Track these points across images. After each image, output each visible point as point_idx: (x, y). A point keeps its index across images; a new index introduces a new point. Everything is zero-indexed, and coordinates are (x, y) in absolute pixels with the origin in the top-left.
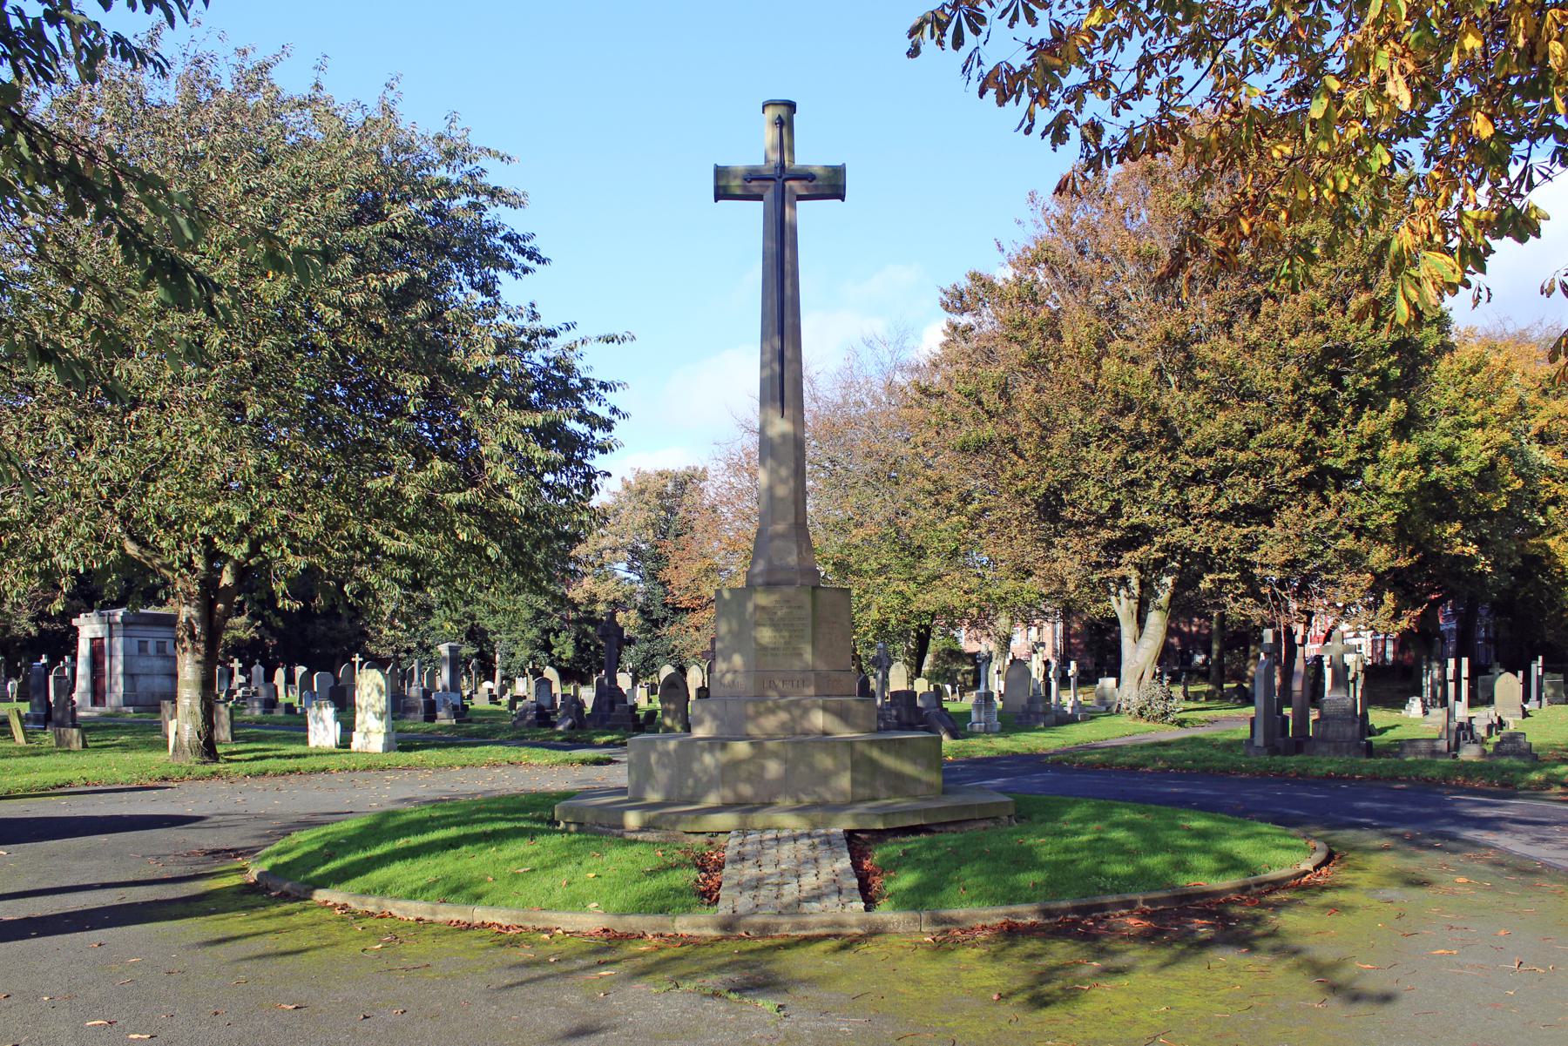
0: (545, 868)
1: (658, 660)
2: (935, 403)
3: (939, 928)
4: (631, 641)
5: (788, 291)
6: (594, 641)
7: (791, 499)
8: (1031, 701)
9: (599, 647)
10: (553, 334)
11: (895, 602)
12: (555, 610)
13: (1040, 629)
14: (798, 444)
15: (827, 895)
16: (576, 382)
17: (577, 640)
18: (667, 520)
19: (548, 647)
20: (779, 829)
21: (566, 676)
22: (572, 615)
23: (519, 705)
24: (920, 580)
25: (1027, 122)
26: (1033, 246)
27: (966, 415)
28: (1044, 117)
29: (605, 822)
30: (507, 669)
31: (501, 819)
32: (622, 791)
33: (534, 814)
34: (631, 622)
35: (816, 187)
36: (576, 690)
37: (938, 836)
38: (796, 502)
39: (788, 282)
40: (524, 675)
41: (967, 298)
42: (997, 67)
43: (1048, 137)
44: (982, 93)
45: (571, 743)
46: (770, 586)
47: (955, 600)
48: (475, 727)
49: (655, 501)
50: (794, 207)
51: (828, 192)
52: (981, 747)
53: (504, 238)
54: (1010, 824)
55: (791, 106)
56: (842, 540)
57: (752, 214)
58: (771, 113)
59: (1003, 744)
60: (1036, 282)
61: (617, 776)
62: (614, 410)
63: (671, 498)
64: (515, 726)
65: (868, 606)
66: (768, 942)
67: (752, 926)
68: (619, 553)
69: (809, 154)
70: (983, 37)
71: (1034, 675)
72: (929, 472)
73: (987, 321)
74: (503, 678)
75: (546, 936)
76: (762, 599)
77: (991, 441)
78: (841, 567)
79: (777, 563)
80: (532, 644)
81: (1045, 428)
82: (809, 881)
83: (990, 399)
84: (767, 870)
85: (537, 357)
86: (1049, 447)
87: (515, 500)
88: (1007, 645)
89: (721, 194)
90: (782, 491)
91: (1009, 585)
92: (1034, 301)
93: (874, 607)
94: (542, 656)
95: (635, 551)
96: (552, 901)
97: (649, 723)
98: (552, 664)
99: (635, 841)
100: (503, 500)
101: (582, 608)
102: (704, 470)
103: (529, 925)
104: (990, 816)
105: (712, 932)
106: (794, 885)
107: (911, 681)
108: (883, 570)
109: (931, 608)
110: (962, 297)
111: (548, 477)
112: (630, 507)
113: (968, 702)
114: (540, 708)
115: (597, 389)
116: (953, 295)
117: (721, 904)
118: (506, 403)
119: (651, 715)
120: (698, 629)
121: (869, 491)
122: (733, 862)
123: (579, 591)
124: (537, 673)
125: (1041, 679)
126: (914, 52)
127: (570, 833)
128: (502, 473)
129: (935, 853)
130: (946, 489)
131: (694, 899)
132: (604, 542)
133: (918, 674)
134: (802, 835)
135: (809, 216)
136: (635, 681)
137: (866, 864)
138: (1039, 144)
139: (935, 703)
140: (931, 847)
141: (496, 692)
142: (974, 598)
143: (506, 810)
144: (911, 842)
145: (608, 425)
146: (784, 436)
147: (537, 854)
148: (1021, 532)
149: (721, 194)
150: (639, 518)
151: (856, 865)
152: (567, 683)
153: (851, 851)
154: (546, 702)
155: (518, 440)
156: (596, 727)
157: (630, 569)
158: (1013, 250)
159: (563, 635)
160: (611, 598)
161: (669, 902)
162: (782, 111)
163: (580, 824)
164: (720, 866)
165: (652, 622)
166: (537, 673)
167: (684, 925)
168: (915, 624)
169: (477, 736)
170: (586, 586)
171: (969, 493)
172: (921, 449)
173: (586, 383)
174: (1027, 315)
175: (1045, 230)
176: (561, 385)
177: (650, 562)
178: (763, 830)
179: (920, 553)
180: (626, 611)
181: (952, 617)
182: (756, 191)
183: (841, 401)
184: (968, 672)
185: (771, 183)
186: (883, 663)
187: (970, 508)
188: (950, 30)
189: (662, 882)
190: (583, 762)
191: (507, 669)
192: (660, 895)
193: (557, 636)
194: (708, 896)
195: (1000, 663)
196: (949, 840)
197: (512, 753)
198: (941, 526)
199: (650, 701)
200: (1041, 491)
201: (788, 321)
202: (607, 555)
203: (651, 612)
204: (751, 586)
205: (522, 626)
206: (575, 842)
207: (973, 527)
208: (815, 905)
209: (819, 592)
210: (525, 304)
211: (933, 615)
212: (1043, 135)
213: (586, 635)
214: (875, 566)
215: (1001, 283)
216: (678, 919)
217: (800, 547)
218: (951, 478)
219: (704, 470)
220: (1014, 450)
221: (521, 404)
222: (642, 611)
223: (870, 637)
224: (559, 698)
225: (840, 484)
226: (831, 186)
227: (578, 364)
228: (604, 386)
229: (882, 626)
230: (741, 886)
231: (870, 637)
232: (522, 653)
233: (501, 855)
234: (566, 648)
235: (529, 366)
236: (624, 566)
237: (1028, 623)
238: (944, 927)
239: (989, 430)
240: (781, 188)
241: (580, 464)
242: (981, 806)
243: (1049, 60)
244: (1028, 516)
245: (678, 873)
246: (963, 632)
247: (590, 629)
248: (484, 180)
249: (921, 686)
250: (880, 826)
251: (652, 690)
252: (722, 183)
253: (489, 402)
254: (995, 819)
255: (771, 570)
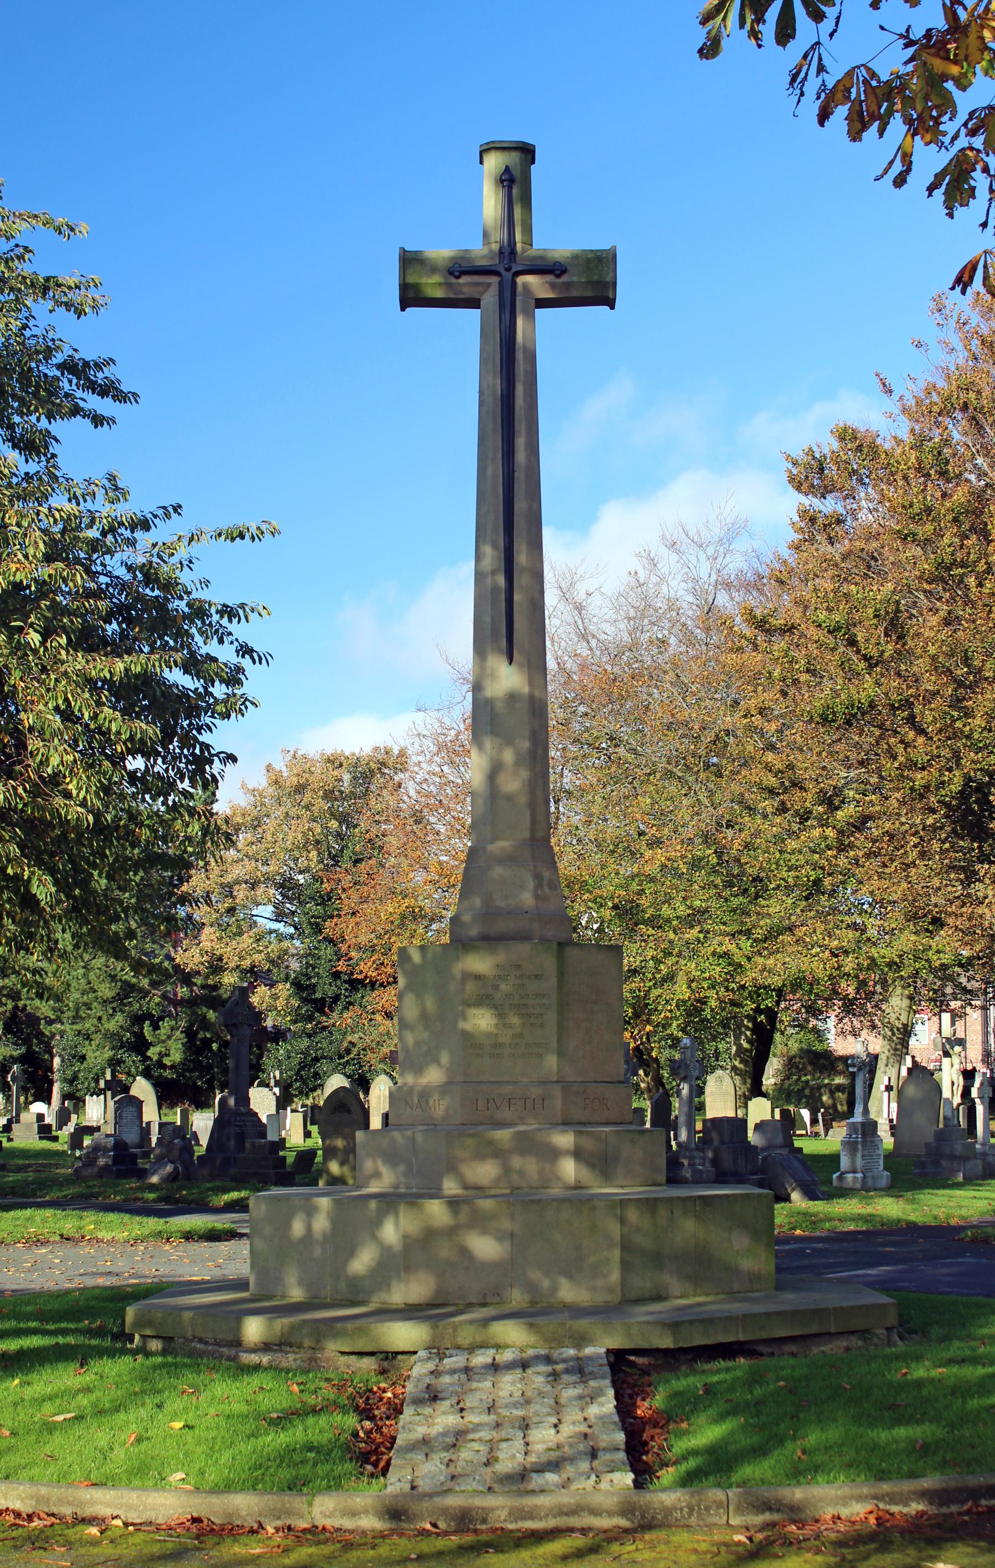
0: (101, 1412)
1: (324, 1066)
2: (780, 644)
3: (759, 1519)
4: (278, 1035)
5: (521, 457)
6: (218, 1038)
7: (523, 799)
8: (941, 1136)
9: (224, 1045)
10: (145, 525)
11: (717, 971)
12: (154, 984)
13: (955, 1016)
14: (537, 708)
15: (572, 1460)
16: (182, 605)
17: (190, 1034)
18: (339, 835)
19: (140, 1046)
20: (498, 1347)
21: (168, 1093)
22: (182, 992)
23: (87, 1141)
24: (758, 933)
25: (898, 167)
26: (941, 384)
27: (831, 663)
28: (930, 160)
29: (209, 1336)
30: (72, 1080)
31: (34, 1332)
32: (241, 1285)
33: (94, 1323)
34: (280, 1003)
35: (568, 285)
36: (185, 1116)
37: (765, 1362)
38: (532, 806)
39: (520, 443)
40: (98, 1092)
41: (832, 471)
42: (850, 74)
43: (939, 194)
44: (823, 116)
45: (171, 1203)
46: (489, 941)
47: (816, 965)
48: (12, 1177)
49: (321, 805)
50: (531, 317)
51: (589, 293)
52: (846, 1211)
53: (61, 367)
54: (890, 1343)
55: (527, 152)
56: (628, 869)
57: (463, 330)
58: (494, 162)
59: (890, 1208)
60: (946, 442)
61: (233, 1259)
62: (245, 650)
63: (348, 799)
64: (77, 1176)
65: (670, 978)
66: (469, 1539)
67: (445, 1512)
68: (260, 890)
69: (557, 232)
70: (827, 25)
71: (946, 1093)
72: (770, 757)
73: (868, 510)
74: (65, 1097)
75: (94, 1531)
76: (479, 963)
77: (872, 706)
78: (628, 913)
79: (500, 903)
80: (114, 1039)
81: (960, 684)
82: (544, 1437)
83: (871, 637)
84: (473, 1418)
85: (115, 564)
86: (968, 714)
87: (77, 801)
88: (905, 1043)
89: (411, 297)
90: (513, 783)
91: (907, 940)
92: (943, 474)
93: (681, 979)
94: (131, 1059)
95: (286, 886)
96: (108, 1468)
97: (304, 1169)
98: (147, 1074)
99: (257, 1368)
100: (59, 801)
101: (198, 981)
102: (402, 753)
103: (67, 1511)
104: (853, 1327)
105: (370, 1523)
106: (519, 1444)
107: (743, 1100)
108: (696, 917)
109: (776, 981)
110: (822, 470)
111: (136, 763)
112: (280, 812)
113: (832, 1140)
114: (120, 1146)
115: (216, 617)
116: (808, 467)
117: (393, 1475)
118: (63, 640)
119: (306, 1157)
120: (389, 1016)
121: (673, 788)
122: (418, 1402)
123: (195, 951)
124: (119, 1088)
125: (957, 1100)
126: (710, 49)
127: (148, 1354)
128: (58, 757)
129: (758, 1392)
130: (797, 784)
131: (349, 1466)
132: (237, 872)
133: (756, 1090)
134: (537, 1358)
135: (556, 336)
136: (283, 1102)
137: (643, 1409)
138: (920, 204)
139: (780, 1140)
140: (753, 1380)
141: (50, 1120)
142: (849, 964)
143: (42, 1316)
144: (720, 1373)
145: (234, 677)
146: (512, 697)
147: (87, 1390)
148: (922, 855)
149: (411, 297)
150: (294, 835)
151: (625, 1409)
152: (172, 1106)
153: (618, 1386)
154: (131, 1137)
155: (83, 704)
156: (212, 1177)
157: (279, 916)
158: (908, 391)
159: (165, 1025)
160: (246, 963)
161: (305, 1470)
162: (512, 158)
163: (167, 1339)
164: (396, 1410)
165: (313, 1003)
166: (119, 1088)
167: (324, 1509)
168: (750, 1006)
169: (14, 1194)
170: (206, 945)
171: (838, 791)
172: (757, 720)
173: (199, 611)
174: (932, 494)
175: (961, 356)
176: (156, 611)
177: (312, 904)
178: (472, 1349)
179: (757, 888)
180: (272, 986)
181: (814, 996)
182: (468, 292)
183: (626, 638)
184: (839, 1088)
185: (494, 280)
186: (695, 1072)
187: (840, 814)
188: (773, 14)
189: (296, 1434)
190: (188, 1236)
191: (72, 1080)
192: (286, 1456)
193: (156, 1027)
194: (371, 1456)
195: (892, 1072)
196: (786, 1366)
197: (68, 1222)
198: (792, 844)
199: (307, 1134)
200: (955, 787)
201: (520, 505)
202: (241, 892)
203: (313, 988)
204: (461, 942)
205: (97, 1010)
206: (155, 1367)
207: (842, 848)
208: (551, 1478)
209: (571, 952)
210: (99, 476)
211: (780, 992)
212: (931, 189)
213: (205, 1024)
214: (682, 910)
215: (887, 446)
216: (318, 1500)
217: (538, 877)
218: (806, 766)
219: (402, 753)
220: (911, 720)
221: (87, 640)
222: (297, 985)
223: (674, 1029)
224: (155, 1129)
225: (623, 775)
226: (590, 282)
227: (185, 577)
228: (229, 612)
229: (694, 1009)
230: (425, 1445)
231: (674, 1029)
232: (98, 1054)
233: (29, 1392)
234: (171, 1047)
235: (103, 579)
236: (268, 910)
237: (939, 1004)
238: (768, 1517)
239: (867, 688)
240: (513, 288)
241: (188, 740)
242: (839, 1311)
243: (938, 65)
244: (935, 828)
245: (323, 1421)
246: (831, 1023)
247: (212, 1015)
248: (26, 269)
249: (760, 1110)
250: (666, 1342)
251: (312, 1116)
252: (411, 279)
253: (34, 638)
254: (863, 1333)
255: (489, 913)
